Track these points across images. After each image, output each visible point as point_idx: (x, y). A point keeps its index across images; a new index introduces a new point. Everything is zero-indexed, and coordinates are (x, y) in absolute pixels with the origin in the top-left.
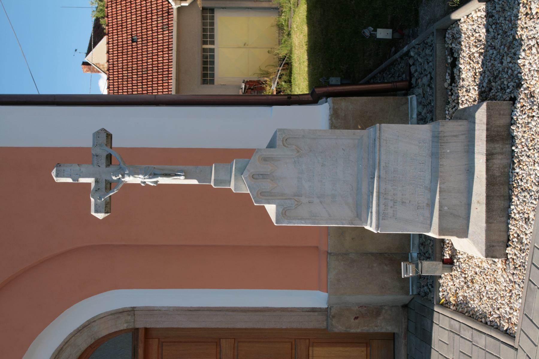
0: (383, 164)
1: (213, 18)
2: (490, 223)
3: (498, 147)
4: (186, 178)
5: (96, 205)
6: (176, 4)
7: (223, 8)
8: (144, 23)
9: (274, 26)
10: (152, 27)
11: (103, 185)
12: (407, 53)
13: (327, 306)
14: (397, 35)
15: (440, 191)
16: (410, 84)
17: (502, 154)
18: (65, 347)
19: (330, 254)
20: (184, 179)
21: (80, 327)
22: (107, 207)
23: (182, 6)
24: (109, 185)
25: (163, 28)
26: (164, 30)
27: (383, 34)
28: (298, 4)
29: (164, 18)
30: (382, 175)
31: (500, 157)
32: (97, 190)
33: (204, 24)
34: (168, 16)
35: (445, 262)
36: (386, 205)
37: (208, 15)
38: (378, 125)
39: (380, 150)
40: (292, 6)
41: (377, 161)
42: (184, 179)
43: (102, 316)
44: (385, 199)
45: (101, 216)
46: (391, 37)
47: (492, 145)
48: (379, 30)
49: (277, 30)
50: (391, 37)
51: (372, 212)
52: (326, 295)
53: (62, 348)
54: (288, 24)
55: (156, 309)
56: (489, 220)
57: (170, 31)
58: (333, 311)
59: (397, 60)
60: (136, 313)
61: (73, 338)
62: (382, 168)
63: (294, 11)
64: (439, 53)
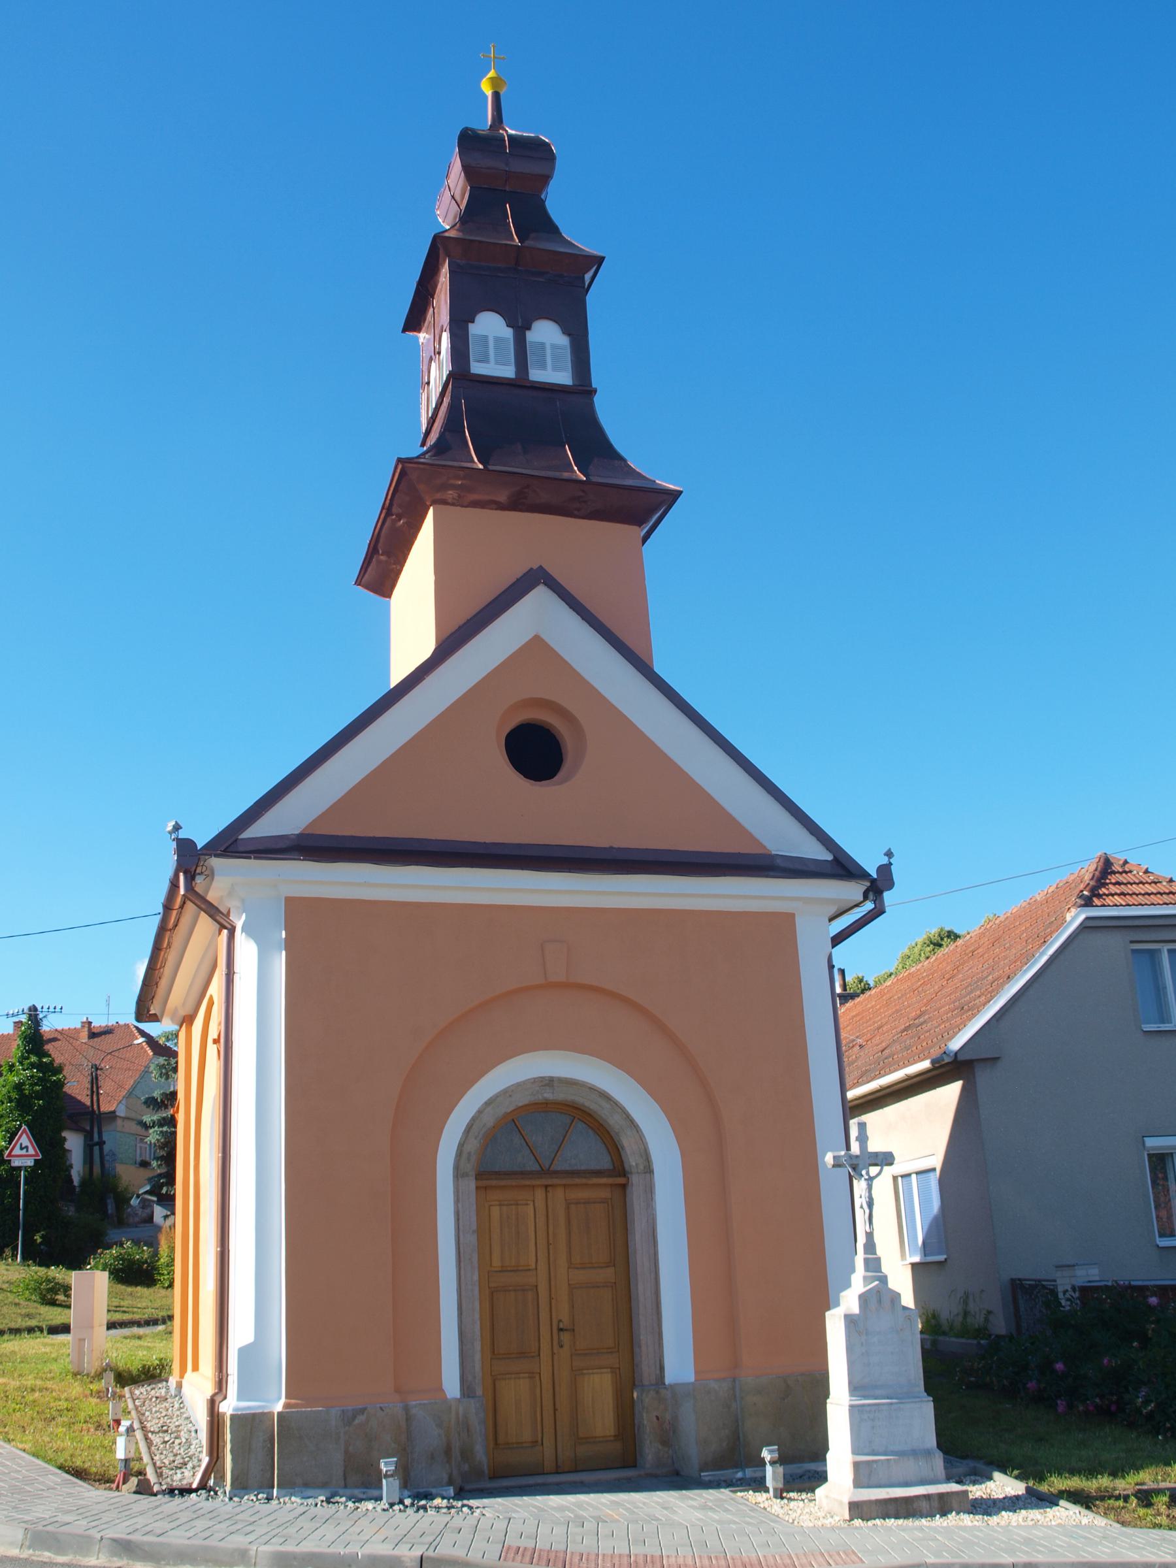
0: (902, 1406)
2: (876, 1504)
3: (936, 1504)
11: (855, 1162)
13: (667, 1383)
15: (888, 1460)
18: (612, 1102)
20: (866, 1232)
21: (632, 1117)
31: (928, 1507)
35: (782, 1491)
36: (870, 1411)
38: (702, 1478)
41: (903, 1401)
42: (866, 1232)
43: (643, 1139)
44: (875, 1411)
47: (936, 1498)
51: (861, 1400)
52: (692, 1379)
53: (610, 1100)
55: (653, 1196)
60: (648, 1175)
61: (621, 1111)
62: (899, 1405)
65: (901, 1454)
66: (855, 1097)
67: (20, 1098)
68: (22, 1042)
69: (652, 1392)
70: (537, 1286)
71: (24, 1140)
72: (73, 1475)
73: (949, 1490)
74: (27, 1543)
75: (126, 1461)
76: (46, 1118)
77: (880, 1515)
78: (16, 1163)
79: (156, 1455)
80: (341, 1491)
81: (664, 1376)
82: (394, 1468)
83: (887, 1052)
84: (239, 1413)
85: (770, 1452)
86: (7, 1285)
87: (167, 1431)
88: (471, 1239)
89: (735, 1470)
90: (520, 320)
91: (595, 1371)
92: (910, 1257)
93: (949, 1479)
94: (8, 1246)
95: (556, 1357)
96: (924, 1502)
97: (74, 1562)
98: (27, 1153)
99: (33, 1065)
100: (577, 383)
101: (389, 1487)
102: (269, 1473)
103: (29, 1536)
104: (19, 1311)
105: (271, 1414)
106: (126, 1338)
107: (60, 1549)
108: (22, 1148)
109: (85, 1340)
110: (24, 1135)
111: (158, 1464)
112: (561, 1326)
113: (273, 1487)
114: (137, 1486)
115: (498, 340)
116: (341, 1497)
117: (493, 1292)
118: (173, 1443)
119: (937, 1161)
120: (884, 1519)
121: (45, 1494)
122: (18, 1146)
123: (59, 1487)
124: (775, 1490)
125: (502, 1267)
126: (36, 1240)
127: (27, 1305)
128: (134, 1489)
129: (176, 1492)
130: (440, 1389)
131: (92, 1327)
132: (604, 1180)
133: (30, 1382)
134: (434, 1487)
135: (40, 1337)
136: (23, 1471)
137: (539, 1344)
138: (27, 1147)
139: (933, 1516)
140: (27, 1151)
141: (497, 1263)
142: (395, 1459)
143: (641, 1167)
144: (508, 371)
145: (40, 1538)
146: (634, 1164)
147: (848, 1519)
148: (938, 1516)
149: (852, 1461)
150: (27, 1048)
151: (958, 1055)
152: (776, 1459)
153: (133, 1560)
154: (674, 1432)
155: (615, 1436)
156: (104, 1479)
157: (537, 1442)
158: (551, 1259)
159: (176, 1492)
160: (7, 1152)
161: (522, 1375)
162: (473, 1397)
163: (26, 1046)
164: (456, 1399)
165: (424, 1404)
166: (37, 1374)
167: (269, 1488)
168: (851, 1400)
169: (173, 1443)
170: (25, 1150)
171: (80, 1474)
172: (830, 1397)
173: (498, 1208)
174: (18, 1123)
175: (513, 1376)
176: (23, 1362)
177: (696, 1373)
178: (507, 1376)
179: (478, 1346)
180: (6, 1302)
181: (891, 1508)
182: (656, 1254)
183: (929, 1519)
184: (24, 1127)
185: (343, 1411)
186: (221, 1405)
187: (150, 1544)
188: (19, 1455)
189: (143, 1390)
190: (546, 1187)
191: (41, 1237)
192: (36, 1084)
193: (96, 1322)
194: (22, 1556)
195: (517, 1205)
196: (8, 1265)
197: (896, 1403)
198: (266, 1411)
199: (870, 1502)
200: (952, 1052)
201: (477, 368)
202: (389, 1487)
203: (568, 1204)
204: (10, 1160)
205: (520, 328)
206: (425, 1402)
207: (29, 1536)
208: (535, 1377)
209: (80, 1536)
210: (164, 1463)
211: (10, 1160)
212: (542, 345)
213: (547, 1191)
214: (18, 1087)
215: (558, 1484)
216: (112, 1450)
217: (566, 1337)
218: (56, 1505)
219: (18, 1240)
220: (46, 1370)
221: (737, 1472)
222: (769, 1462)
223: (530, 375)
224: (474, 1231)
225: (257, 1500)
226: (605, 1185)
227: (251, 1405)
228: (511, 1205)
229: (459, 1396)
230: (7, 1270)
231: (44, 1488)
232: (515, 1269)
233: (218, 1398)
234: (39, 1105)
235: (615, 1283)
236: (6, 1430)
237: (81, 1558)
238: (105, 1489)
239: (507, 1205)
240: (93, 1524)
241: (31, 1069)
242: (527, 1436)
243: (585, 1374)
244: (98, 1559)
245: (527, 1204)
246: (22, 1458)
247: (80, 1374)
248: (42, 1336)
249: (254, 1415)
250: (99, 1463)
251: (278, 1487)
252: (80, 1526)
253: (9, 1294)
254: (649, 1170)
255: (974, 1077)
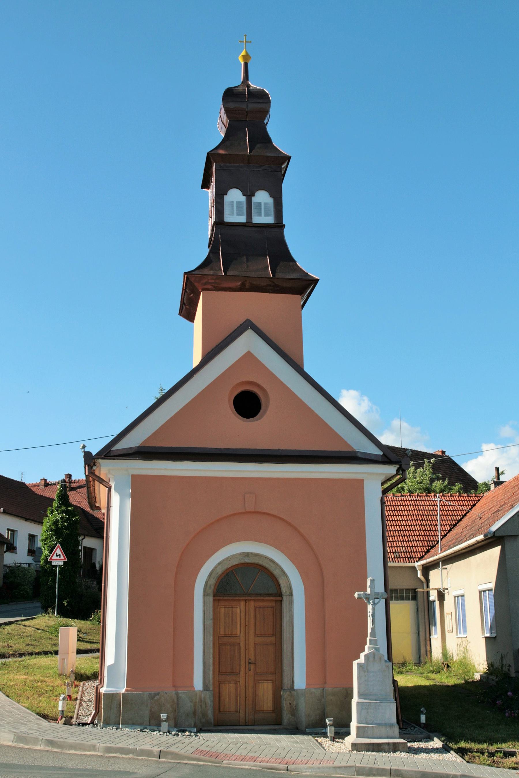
0: (381, 704)
1: (408, 599)
2: (364, 745)
3: (391, 747)
4: (371, 628)
5: (360, 594)
6: (419, 566)
7: (417, 609)
8: (399, 534)
9: (404, 659)
10: (396, 542)
12: (415, 728)
13: (295, 689)
14: (422, 725)
15: (373, 727)
16: (402, 728)
17: (389, 748)
19: (324, 689)
22: (360, 598)
23: (417, 571)
24: (368, 599)
25: (396, 552)
26: (395, 553)
27: (423, 718)
28: (428, 679)
29: (405, 553)
30: (377, 704)
31: (388, 748)
32: (366, 594)
33: (402, 590)
34: (407, 558)
36: (366, 705)
37: (410, 595)
39: (386, 703)
40: (425, 675)
45: (356, 595)
46: (421, 722)
47: (392, 745)
48: (425, 716)
49: (402, 662)
50: (421, 722)
53: (275, 563)
54: (408, 672)
56: (365, 744)
57: (394, 559)
58: (293, 692)
59: (411, 725)
60: (290, 596)
63: (422, 677)
64: (419, 736)
65: (379, 725)
66: (461, 549)
67: (56, 529)
68: (58, 499)
69: (288, 692)
70: (240, 644)
71: (58, 551)
72: (42, 717)
73: (398, 742)
74: (15, 740)
75: (62, 711)
76: (70, 540)
77: (365, 749)
78: (54, 563)
79: (80, 711)
80: (148, 727)
81: (294, 686)
82: (166, 718)
83: (483, 524)
84: (107, 693)
85: (329, 720)
86: (47, 628)
87: (91, 701)
88: (210, 623)
89: (322, 729)
90: (249, 192)
91: (264, 682)
92: (463, 634)
93: (401, 737)
94: (50, 607)
95: (247, 675)
96: (386, 746)
97: (31, 748)
98: (60, 558)
99: (63, 512)
100: (276, 222)
101: (164, 726)
102: (118, 718)
103: (15, 737)
104: (51, 642)
105: (120, 693)
106: (94, 658)
107: (27, 743)
108: (57, 556)
109: (65, 659)
110: (58, 548)
111: (80, 714)
112: (250, 661)
113: (120, 724)
114: (64, 721)
115: (238, 203)
116: (147, 729)
117: (220, 645)
118: (91, 706)
119: (492, 586)
120: (367, 751)
121: (27, 723)
122: (55, 554)
123: (33, 721)
124: (331, 737)
125: (225, 635)
126: (64, 604)
127: (55, 639)
128: (63, 722)
129: (81, 724)
130: (192, 686)
131: (68, 653)
132: (271, 598)
133: (37, 678)
134: (188, 728)
135: (50, 657)
136: (21, 715)
137: (240, 669)
138: (60, 555)
139: (389, 752)
140: (60, 557)
141: (222, 633)
142: (167, 714)
143: (288, 593)
144: (242, 219)
145: (20, 738)
146: (285, 591)
147: (351, 750)
148: (392, 752)
149: (356, 726)
150: (60, 502)
151: (495, 533)
152: (332, 724)
153: (53, 748)
154: (297, 710)
155: (272, 711)
156: (55, 719)
157: (237, 711)
158: (247, 632)
159: (81, 724)
160: (49, 558)
161: (232, 682)
162: (208, 690)
163: (59, 501)
164: (201, 691)
165: (185, 692)
166: (43, 674)
167: (118, 724)
168: (358, 700)
169: (91, 706)
170: (59, 556)
171: (45, 717)
172: (354, 698)
173: (224, 609)
174: (55, 542)
175: (228, 682)
176: (38, 669)
177: (306, 685)
178: (225, 682)
179: (211, 668)
180: (45, 637)
181: (371, 748)
182: (293, 631)
183: (387, 753)
184: (58, 544)
185: (150, 694)
186: (101, 689)
187: (60, 742)
188: (21, 708)
189: (90, 683)
190: (246, 600)
191: (67, 603)
192: (65, 522)
193: (70, 651)
194: (12, 745)
195: (233, 608)
196: (50, 617)
197: (379, 703)
198: (118, 692)
199: (361, 744)
200: (492, 532)
201: (228, 219)
202: (164, 726)
203: (255, 608)
204: (51, 562)
205: (249, 195)
206: (186, 691)
207: (15, 737)
208: (237, 683)
209: (34, 738)
210: (82, 714)
211: (51, 562)
212: (260, 204)
213: (246, 602)
214: (56, 523)
215: (243, 730)
216: (57, 707)
217: (252, 666)
218: (30, 727)
219: (55, 604)
220: (47, 672)
221: (323, 729)
222: (329, 725)
223: (253, 220)
224: (211, 619)
225: (113, 729)
226: (272, 600)
227: (112, 690)
228: (230, 608)
229: (202, 690)
230: (49, 620)
231: (27, 721)
232: (230, 636)
233: (99, 687)
234: (66, 532)
235: (275, 643)
236: (20, 698)
237: (34, 747)
238: (54, 723)
239: (228, 608)
240: (41, 734)
241: (62, 513)
242: (233, 709)
243: (260, 683)
244: (40, 747)
245: (237, 608)
246: (22, 709)
247: (62, 675)
248: (52, 656)
249: (113, 694)
250: (54, 713)
251: (122, 724)
252: (36, 734)
253: (47, 633)
254: (291, 594)
255: (504, 543)
